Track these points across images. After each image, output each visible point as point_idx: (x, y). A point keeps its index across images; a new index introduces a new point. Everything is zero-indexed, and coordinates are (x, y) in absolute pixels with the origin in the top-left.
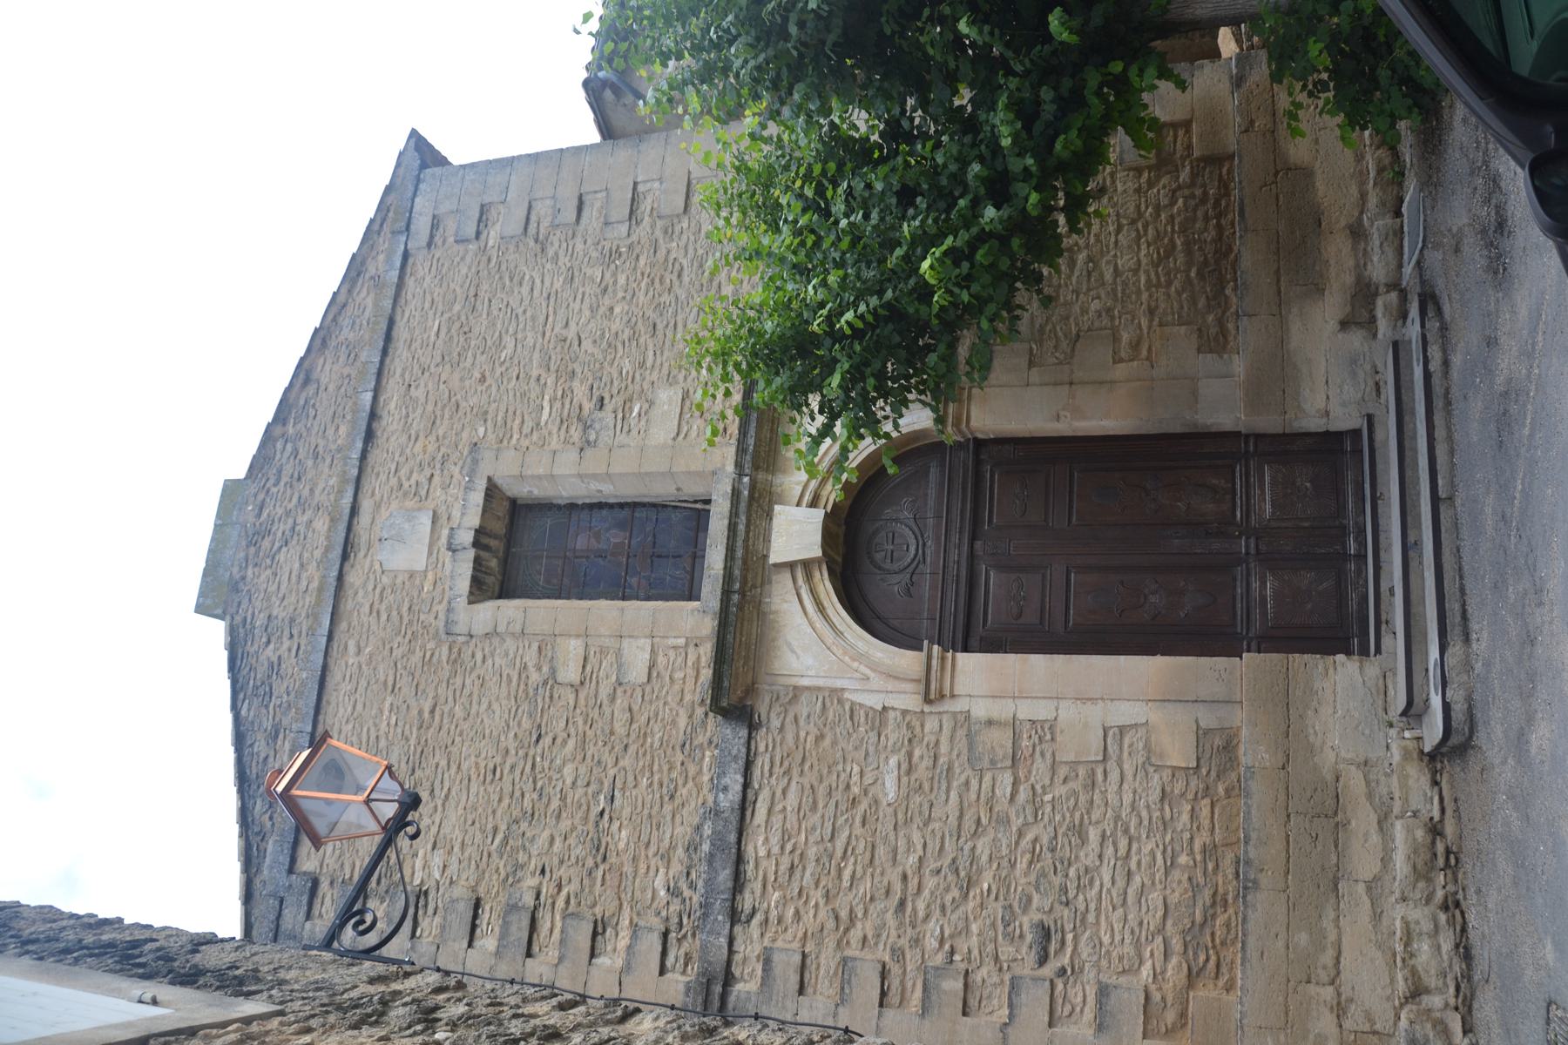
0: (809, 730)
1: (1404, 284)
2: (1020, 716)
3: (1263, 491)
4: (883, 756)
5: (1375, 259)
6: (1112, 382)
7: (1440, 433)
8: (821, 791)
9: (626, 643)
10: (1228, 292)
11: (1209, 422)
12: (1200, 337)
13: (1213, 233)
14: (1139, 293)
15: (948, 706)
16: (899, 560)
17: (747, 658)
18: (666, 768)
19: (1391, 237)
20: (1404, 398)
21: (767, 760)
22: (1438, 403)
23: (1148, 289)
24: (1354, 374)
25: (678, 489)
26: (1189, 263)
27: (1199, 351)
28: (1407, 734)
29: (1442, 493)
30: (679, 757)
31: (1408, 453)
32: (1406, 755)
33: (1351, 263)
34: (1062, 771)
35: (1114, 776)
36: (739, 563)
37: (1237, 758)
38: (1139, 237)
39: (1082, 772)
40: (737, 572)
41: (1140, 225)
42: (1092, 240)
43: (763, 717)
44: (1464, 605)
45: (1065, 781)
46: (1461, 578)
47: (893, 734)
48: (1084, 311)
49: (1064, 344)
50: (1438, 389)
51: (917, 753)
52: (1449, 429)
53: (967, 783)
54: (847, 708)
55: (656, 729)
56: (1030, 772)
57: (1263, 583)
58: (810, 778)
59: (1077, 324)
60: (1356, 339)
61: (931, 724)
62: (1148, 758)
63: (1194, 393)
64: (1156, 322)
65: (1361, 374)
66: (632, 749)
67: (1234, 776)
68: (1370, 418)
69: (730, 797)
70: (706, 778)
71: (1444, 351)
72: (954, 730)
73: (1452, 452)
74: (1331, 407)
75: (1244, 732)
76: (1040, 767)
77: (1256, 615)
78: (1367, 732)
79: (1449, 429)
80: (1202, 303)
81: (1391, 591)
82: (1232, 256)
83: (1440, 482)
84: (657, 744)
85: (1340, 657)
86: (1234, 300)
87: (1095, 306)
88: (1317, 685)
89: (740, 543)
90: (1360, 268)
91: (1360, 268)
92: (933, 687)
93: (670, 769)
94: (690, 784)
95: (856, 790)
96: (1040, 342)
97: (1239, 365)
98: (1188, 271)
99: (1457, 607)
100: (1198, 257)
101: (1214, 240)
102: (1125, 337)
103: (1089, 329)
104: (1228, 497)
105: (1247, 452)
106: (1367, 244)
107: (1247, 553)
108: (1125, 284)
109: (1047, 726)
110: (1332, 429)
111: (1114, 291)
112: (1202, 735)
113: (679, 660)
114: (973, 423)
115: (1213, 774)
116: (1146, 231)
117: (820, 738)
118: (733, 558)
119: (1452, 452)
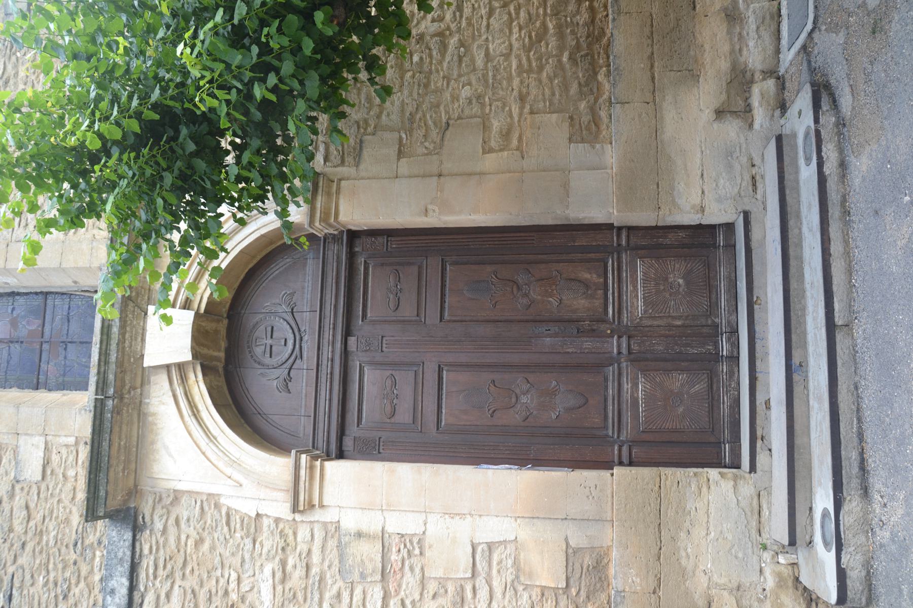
0: (190, 531)
1: (782, 71)
2: (390, 529)
3: (635, 287)
4: (258, 564)
5: (751, 44)
6: (481, 174)
7: (836, 248)
8: (202, 596)
9: (22, 440)
10: (601, 77)
11: (581, 216)
12: (572, 125)
13: (586, 16)
14: (510, 79)
15: (318, 515)
16: (278, 354)
17: (127, 461)
18: (60, 566)
19: (767, 21)
20: (789, 199)
21: (151, 563)
22: (834, 212)
23: (519, 74)
24: (730, 167)
25: (75, 282)
26: (561, 48)
27: (570, 140)
28: (782, 559)
29: (839, 320)
30: (73, 556)
31: (793, 263)
32: (781, 582)
33: (726, 48)
34: (432, 587)
35: (483, 593)
36: (113, 367)
37: (607, 577)
38: (511, 20)
39: (451, 588)
40: (111, 377)
41: (512, 8)
42: (464, 24)
43: (147, 519)
44: (862, 453)
45: (434, 596)
46: (859, 420)
47: (268, 541)
48: (455, 98)
49: (434, 134)
50: (834, 196)
51: (291, 562)
52: (846, 243)
53: (339, 595)
54: (224, 513)
55: (51, 528)
56: (400, 586)
57: (635, 385)
58: (191, 582)
59: (447, 112)
60: (731, 128)
61: (303, 533)
62: (517, 577)
63: (566, 185)
64: (527, 109)
65: (737, 167)
66: (29, 547)
67: (603, 597)
68: (746, 215)
69: (117, 600)
70: (97, 578)
71: (841, 151)
72: (325, 540)
73: (849, 271)
74: (706, 202)
75: (614, 554)
76: (410, 581)
77: (627, 418)
78: (740, 555)
79: (846, 243)
80: (574, 89)
81: (767, 404)
82: (605, 40)
83: (837, 306)
84: (52, 543)
85: (713, 473)
86: (607, 86)
87: (466, 92)
88: (690, 505)
89: (113, 347)
90: (735, 53)
91: (735, 53)
92: (301, 498)
93: (64, 568)
94: (82, 584)
95: (234, 596)
96: (411, 130)
97: (611, 156)
98: (559, 56)
99: (854, 455)
100: (571, 41)
101: (586, 24)
102: (496, 124)
103: (459, 118)
104: (600, 292)
105: (619, 245)
106: (742, 29)
107: (619, 353)
108: (496, 69)
109: (415, 540)
110: (704, 222)
111: (485, 76)
112: (571, 554)
113: (71, 458)
114: (342, 218)
115: (583, 594)
116: (518, 14)
117: (199, 542)
118: (107, 363)
119: (849, 271)
